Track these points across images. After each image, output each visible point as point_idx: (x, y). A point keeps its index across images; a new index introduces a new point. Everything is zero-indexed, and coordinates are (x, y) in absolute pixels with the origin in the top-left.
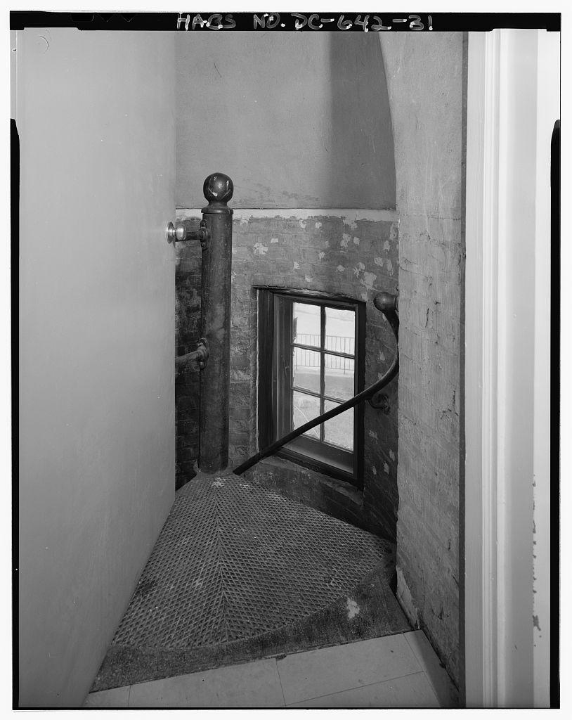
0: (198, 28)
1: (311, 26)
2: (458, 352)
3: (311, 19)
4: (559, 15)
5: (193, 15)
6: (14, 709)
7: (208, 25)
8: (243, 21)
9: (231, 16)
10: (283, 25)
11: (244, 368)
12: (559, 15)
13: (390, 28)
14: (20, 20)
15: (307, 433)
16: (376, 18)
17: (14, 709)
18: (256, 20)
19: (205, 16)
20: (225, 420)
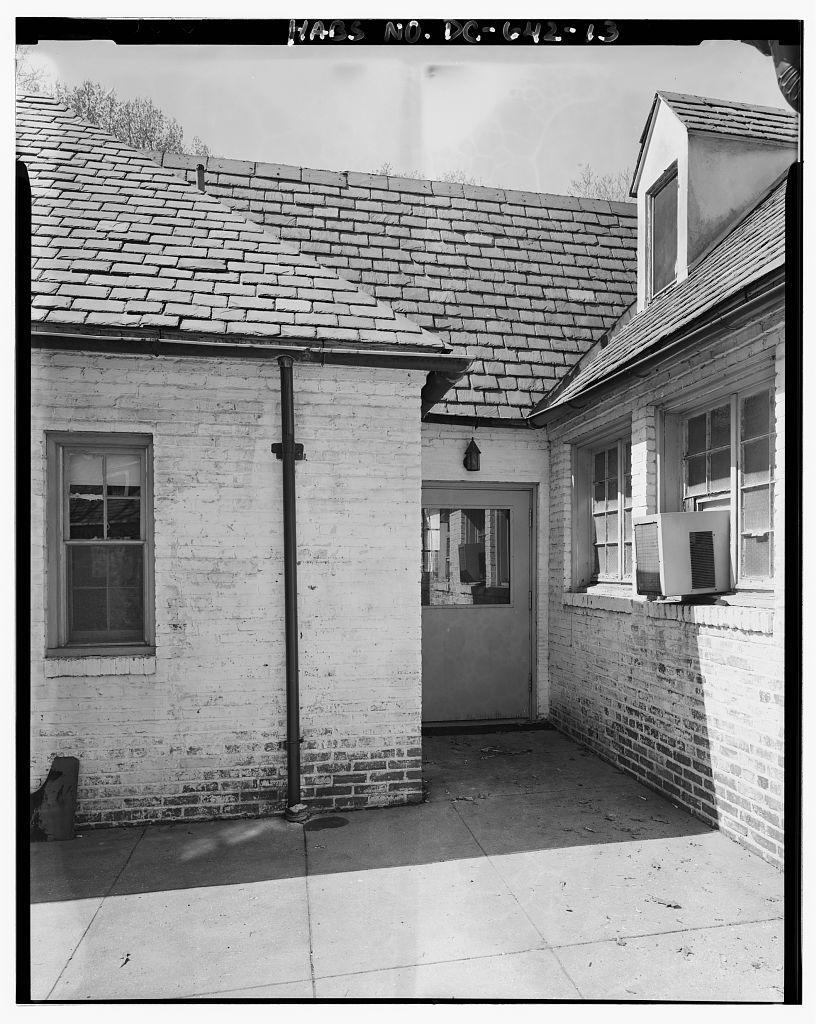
0: (317, 41)
1: (466, 37)
2: (726, 534)
3: (467, 27)
4: (18, 20)
5: (312, 22)
6: (19, 1001)
7: (332, 34)
8: (373, 32)
9: (359, 23)
10: (427, 36)
11: (218, 573)
12: (18, 20)
13: (558, 39)
14: (30, 31)
15: (34, 784)
16: (550, 24)
17: (19, 1001)
18: (390, 29)
19: (327, 24)
20: (554, 545)
